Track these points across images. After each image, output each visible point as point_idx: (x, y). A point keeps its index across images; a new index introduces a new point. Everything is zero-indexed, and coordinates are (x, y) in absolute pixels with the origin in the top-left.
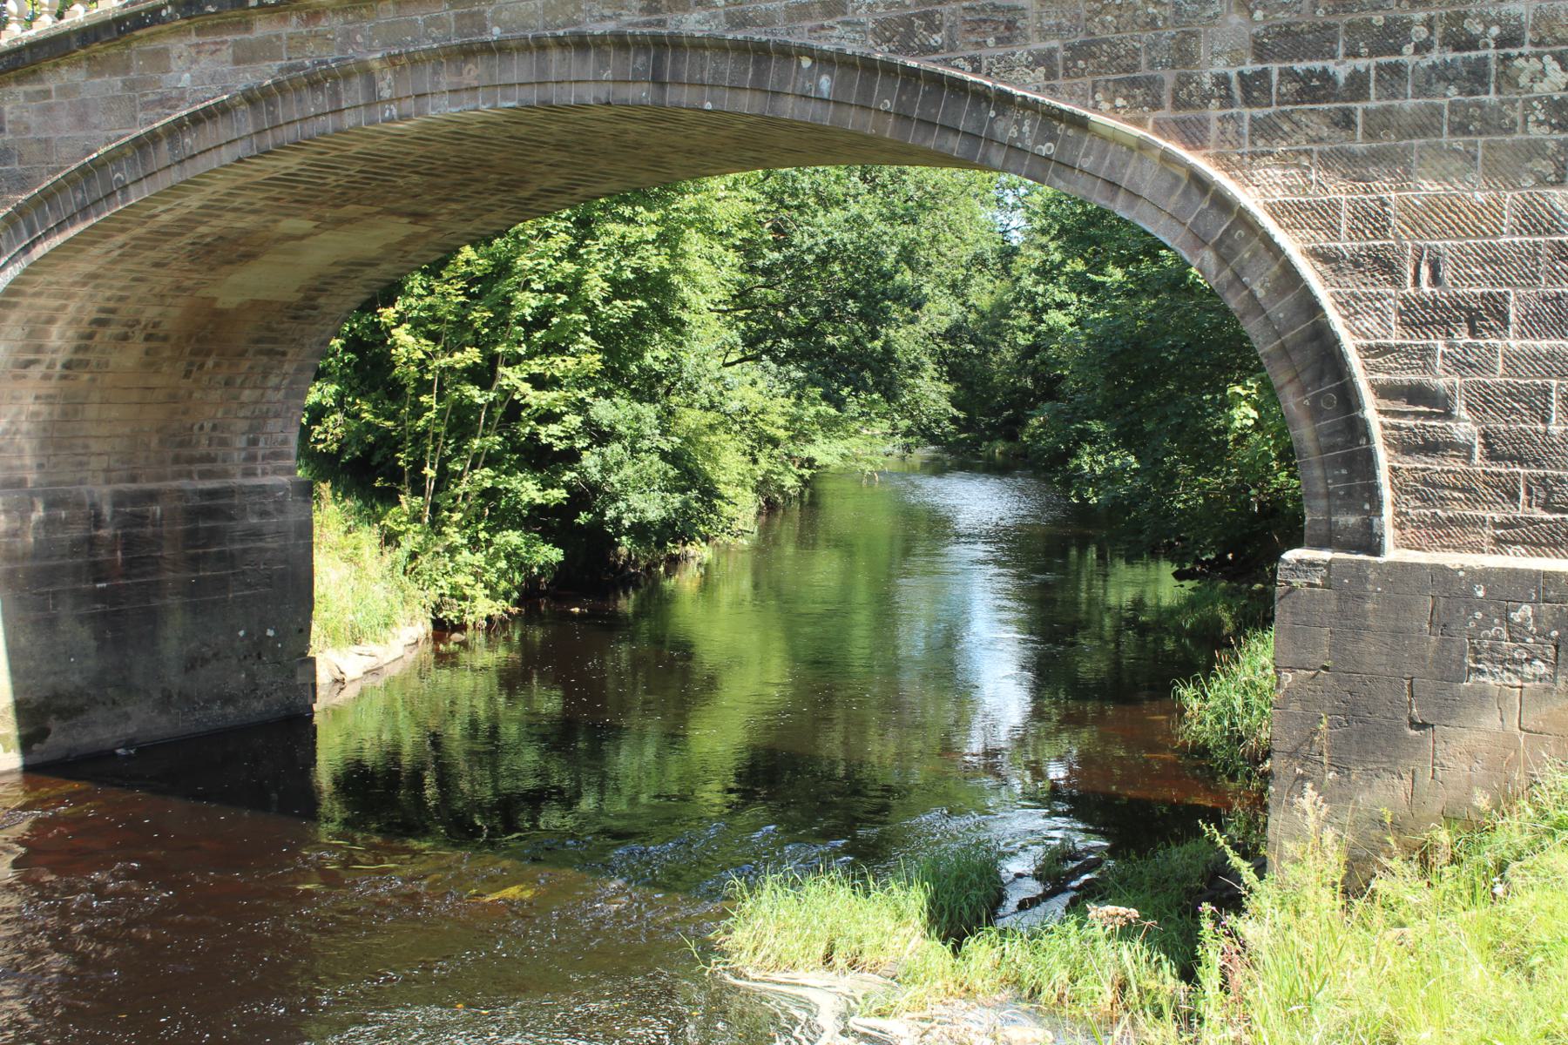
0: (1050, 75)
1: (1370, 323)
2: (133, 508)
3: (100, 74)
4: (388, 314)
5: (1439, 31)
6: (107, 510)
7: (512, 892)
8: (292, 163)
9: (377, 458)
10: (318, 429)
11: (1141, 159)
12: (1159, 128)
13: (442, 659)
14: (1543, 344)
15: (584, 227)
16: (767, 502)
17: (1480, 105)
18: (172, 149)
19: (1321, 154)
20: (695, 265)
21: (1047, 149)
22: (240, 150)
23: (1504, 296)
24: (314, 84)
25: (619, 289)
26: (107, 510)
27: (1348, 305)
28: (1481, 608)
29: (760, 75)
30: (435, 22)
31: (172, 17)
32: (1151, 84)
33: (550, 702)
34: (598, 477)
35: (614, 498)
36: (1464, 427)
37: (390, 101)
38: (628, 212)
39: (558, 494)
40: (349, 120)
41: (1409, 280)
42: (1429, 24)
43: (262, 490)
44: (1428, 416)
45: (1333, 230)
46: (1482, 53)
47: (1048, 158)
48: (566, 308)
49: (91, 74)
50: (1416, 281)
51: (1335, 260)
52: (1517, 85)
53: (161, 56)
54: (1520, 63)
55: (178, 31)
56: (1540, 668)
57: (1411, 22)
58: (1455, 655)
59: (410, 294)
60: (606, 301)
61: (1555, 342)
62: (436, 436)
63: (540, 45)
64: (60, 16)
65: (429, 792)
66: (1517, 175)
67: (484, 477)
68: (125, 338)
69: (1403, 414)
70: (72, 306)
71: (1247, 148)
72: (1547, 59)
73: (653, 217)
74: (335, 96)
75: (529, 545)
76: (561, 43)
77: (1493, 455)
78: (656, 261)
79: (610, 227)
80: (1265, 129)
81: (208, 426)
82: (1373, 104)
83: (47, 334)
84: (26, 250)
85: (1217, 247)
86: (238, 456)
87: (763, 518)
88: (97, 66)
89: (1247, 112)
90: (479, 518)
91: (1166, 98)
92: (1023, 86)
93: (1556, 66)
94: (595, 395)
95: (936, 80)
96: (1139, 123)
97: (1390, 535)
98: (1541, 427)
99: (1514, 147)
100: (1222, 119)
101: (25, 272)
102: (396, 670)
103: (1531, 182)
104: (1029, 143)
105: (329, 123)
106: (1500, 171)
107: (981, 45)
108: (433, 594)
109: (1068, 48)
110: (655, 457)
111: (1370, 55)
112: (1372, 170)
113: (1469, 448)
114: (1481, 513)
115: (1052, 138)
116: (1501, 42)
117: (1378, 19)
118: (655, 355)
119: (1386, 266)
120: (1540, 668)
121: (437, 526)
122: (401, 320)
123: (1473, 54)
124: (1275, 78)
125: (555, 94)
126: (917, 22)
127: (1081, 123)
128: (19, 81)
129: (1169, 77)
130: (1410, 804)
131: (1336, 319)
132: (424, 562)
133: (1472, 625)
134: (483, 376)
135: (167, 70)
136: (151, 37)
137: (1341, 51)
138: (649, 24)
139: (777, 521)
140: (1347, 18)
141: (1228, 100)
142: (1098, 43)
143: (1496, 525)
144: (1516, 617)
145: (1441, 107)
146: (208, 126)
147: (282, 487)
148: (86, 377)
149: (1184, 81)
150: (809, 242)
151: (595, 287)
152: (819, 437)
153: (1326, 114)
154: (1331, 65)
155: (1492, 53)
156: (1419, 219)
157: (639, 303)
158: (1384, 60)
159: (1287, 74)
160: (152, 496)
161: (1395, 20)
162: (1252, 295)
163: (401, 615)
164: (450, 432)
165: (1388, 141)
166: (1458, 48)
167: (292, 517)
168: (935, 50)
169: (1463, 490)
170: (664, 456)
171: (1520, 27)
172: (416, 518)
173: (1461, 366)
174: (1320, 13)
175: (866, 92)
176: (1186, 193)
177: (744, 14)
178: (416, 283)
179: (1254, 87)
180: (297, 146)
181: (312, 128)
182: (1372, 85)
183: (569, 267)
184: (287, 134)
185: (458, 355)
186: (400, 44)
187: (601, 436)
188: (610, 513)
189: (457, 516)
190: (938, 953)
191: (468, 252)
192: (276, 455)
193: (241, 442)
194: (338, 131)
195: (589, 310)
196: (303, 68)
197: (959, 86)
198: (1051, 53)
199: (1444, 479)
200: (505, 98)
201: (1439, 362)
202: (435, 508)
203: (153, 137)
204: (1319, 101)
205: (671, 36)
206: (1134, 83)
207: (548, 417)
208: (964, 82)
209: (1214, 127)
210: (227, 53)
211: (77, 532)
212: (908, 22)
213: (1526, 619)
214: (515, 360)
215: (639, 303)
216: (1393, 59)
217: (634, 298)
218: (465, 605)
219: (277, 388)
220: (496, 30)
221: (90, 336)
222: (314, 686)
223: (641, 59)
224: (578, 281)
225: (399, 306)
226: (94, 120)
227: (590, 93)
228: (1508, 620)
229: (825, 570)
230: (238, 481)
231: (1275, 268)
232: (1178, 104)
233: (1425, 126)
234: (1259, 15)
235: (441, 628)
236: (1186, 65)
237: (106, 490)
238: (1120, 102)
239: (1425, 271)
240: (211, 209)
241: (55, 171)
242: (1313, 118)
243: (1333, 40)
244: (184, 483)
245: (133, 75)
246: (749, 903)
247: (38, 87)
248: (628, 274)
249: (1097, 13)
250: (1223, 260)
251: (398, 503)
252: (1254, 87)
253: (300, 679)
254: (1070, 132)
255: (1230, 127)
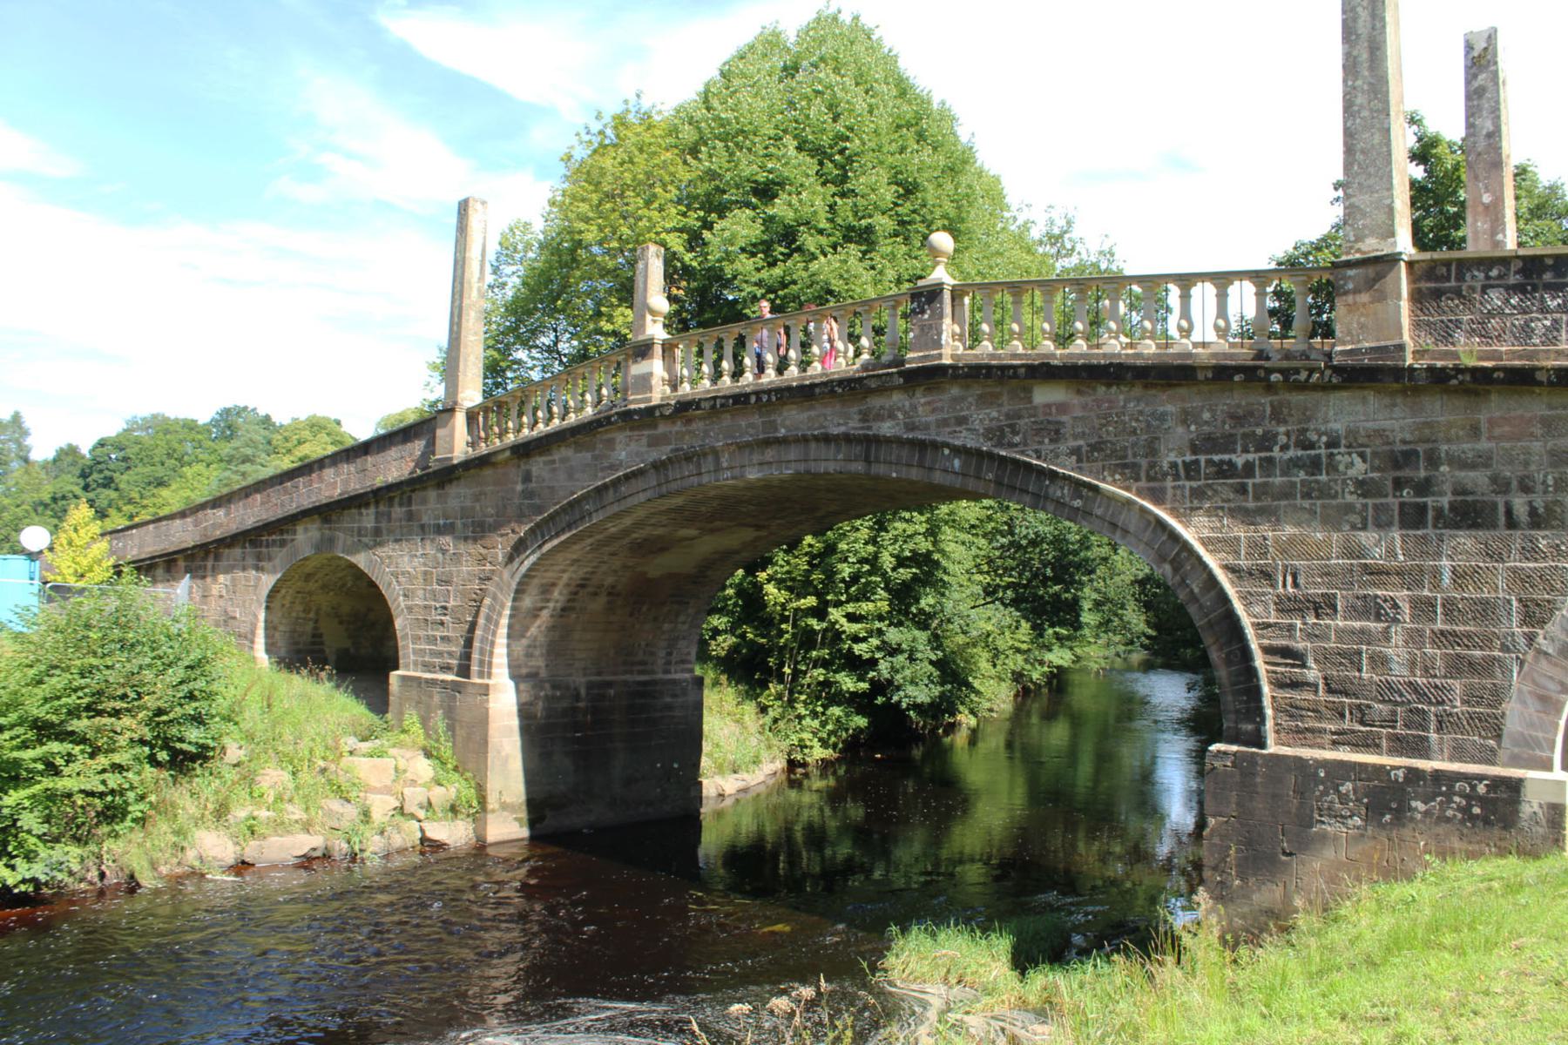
0: (1079, 460)
1: (1258, 609)
2: (598, 690)
3: (580, 452)
4: (762, 576)
5: (1293, 438)
6: (583, 692)
7: (779, 927)
8: (678, 501)
9: (758, 660)
10: (713, 642)
11: (1129, 510)
12: (1139, 494)
13: (794, 784)
14: (1357, 624)
15: (881, 526)
16: (1023, 688)
17: (1317, 482)
18: (615, 492)
19: (1230, 509)
20: (950, 547)
21: (1077, 503)
22: (649, 494)
23: (1334, 595)
24: (688, 458)
25: (901, 562)
26: (583, 692)
27: (1246, 598)
28: (1322, 783)
29: (922, 458)
30: (752, 425)
31: (616, 421)
32: (1135, 467)
33: (856, 812)
34: (888, 676)
35: (898, 688)
36: (1313, 673)
37: (727, 469)
38: (907, 515)
39: (864, 686)
40: (705, 479)
41: (1280, 583)
42: (1288, 434)
43: (674, 682)
44: (1293, 666)
45: (1237, 553)
46: (1317, 452)
47: (1078, 509)
48: (870, 573)
49: (576, 452)
50: (1284, 585)
51: (1239, 571)
52: (1337, 470)
53: (610, 444)
54: (1339, 458)
55: (621, 429)
56: (1357, 821)
57: (1278, 433)
58: (1308, 812)
59: (776, 564)
60: (894, 569)
61: (1363, 623)
62: (792, 649)
63: (805, 440)
64: (563, 419)
65: (781, 865)
66: (1340, 524)
67: (819, 674)
68: (596, 594)
69: (1278, 665)
70: (566, 576)
71: (1188, 505)
72: (1354, 455)
73: (923, 519)
74: (699, 465)
75: (847, 715)
76: (816, 438)
77: (1330, 691)
78: (924, 545)
79: (898, 524)
80: (1198, 494)
81: (643, 643)
82: (1258, 480)
83: (552, 593)
84: (540, 547)
85: (1172, 562)
86: (660, 662)
87: (1020, 699)
88: (579, 447)
89: (1188, 484)
90: (818, 699)
91: (1143, 475)
92: (1064, 467)
93: (1359, 460)
94: (889, 625)
95: (1016, 462)
96: (1127, 489)
97: (1271, 738)
98: (1357, 674)
99: (1338, 507)
100: (1174, 488)
101: (539, 559)
102: (762, 789)
103: (1348, 527)
104: (1067, 499)
105: (695, 480)
106: (1331, 521)
107: (1041, 443)
108: (785, 745)
109: (1088, 445)
110: (926, 663)
111: (1255, 452)
112: (1258, 519)
113: (1316, 686)
114: (1323, 725)
115: (1081, 497)
116: (1329, 445)
117: (1259, 431)
118: (927, 601)
119: (1267, 575)
120: (1357, 821)
121: (791, 702)
122: (769, 581)
123: (1313, 452)
124: (1203, 464)
125: (814, 467)
126: (1007, 430)
127: (1095, 489)
128: (541, 454)
129: (1144, 463)
130: (1283, 903)
131: (1239, 607)
132: (781, 724)
133: (1317, 793)
134: (820, 612)
135: (613, 450)
136: (606, 432)
137: (1239, 449)
138: (862, 428)
139: (1029, 702)
140: (1242, 431)
141: (1177, 477)
142: (1103, 442)
143: (1333, 733)
144: (1343, 789)
145: (1295, 483)
146: (633, 481)
147: (685, 680)
148: (574, 616)
149: (1152, 465)
150: (1024, 532)
151: (887, 561)
152: (1056, 648)
153: (1231, 485)
154: (1233, 457)
155: (1323, 451)
156: (1285, 549)
157: (914, 570)
158: (1263, 455)
159: (1209, 462)
160: (609, 684)
161: (1269, 432)
162: (1192, 591)
163: (765, 755)
164: (800, 648)
165: (1267, 502)
166: (1305, 448)
167: (691, 698)
168: (1016, 445)
169: (1313, 711)
170: (931, 662)
171: (1338, 437)
172: (779, 697)
173: (1310, 636)
174: (1227, 427)
175: (979, 468)
176: (1154, 531)
177: (913, 423)
178: (780, 557)
179: (1191, 470)
180: (678, 492)
181: (687, 483)
182: (1257, 469)
183: (871, 548)
184: (674, 486)
185: (803, 601)
186: (734, 437)
187: (893, 651)
188: (895, 698)
189: (803, 697)
190: (1012, 976)
191: (809, 539)
192: (683, 662)
193: (662, 653)
194: (700, 485)
195: (884, 575)
196: (682, 449)
197: (1029, 466)
198: (1079, 448)
199: (1303, 704)
200: (787, 468)
201: (1298, 633)
202: (791, 692)
203: (605, 487)
204: (1226, 478)
205: (874, 435)
206: (1125, 466)
207: (856, 639)
208: (1030, 464)
209: (1170, 492)
210: (644, 441)
211: (565, 704)
212: (1001, 429)
213: (1348, 791)
214: (838, 604)
215: (914, 570)
216: (1268, 454)
217: (911, 567)
218: (806, 751)
219: (684, 623)
220: (783, 431)
221: (576, 593)
222: (701, 798)
223: (859, 448)
224: (876, 556)
225: (769, 571)
226: (577, 476)
227: (832, 467)
228: (1339, 791)
229: (1058, 735)
230: (660, 676)
231: (1205, 576)
232: (1150, 479)
233: (1287, 493)
234: (1193, 428)
235: (792, 764)
236: (1154, 456)
237: (583, 680)
238: (1117, 477)
239: (1289, 579)
240: (639, 525)
241: (556, 504)
242: (1224, 487)
243: (1235, 443)
244: (628, 677)
245: (597, 452)
246: (901, 943)
247: (550, 458)
248: (907, 554)
249: (1104, 425)
250: (1176, 570)
251: (768, 688)
252: (1191, 470)
253: (693, 794)
254: (1090, 494)
255: (1178, 492)
